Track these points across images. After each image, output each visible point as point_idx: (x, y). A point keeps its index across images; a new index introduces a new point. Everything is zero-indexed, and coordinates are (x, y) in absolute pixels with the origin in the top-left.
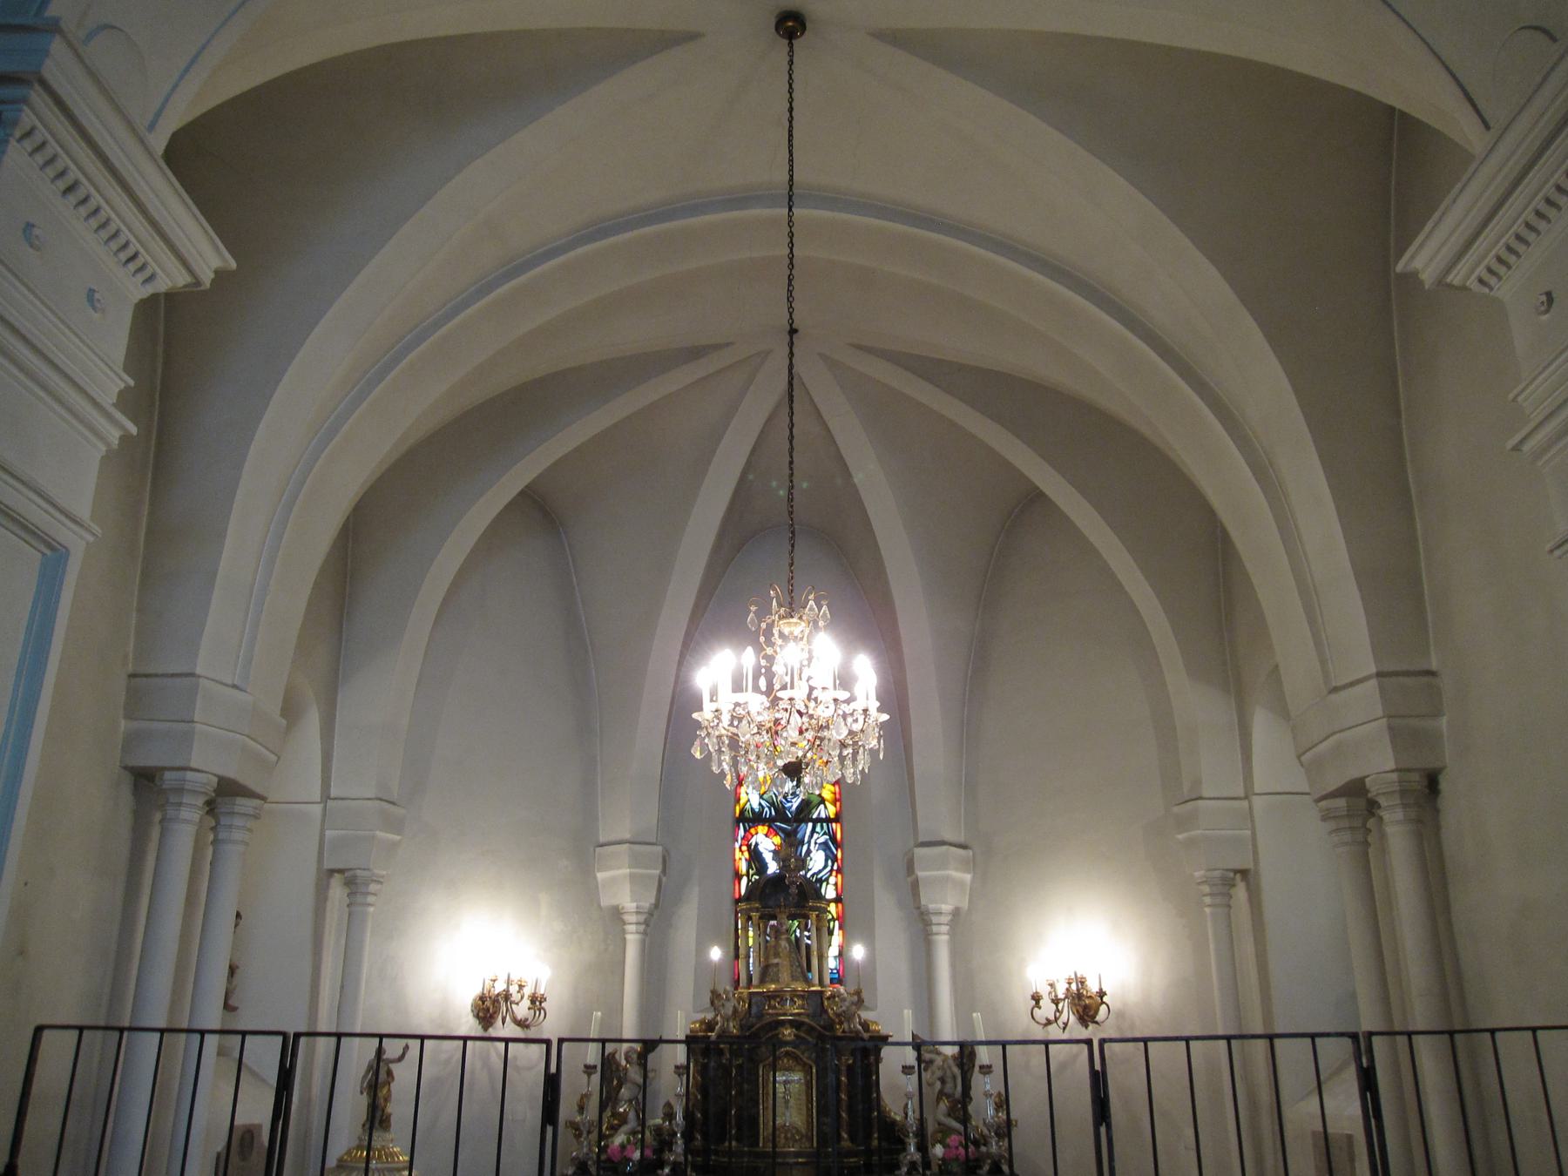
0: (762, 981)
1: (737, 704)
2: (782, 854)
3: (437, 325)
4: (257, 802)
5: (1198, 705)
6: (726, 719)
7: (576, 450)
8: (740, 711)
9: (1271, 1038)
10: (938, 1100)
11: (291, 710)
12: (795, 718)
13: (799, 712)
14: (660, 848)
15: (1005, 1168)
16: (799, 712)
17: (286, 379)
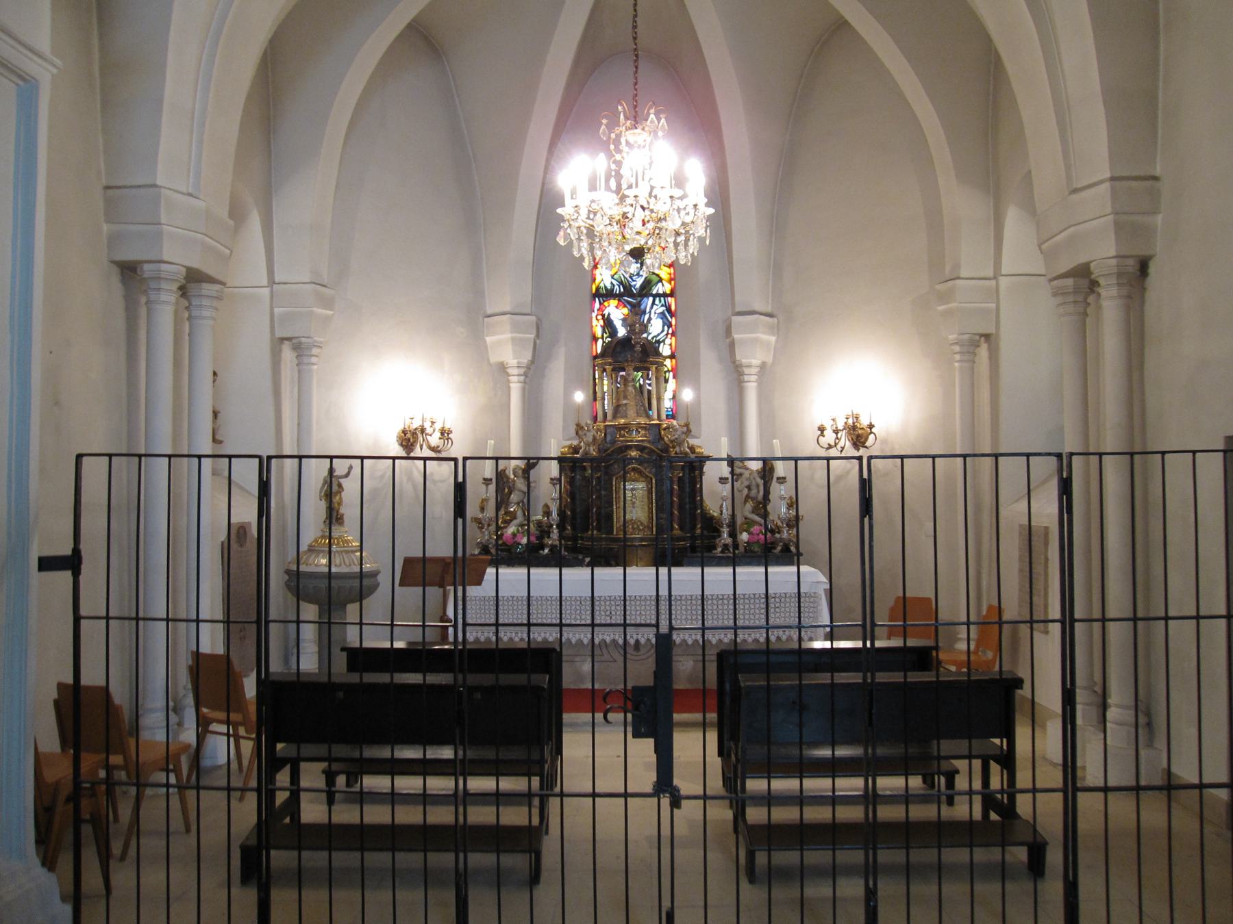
0: (615, 417)
1: (593, 201)
2: (629, 321)
4: (217, 287)
5: (962, 204)
8: (594, 206)
9: (996, 456)
11: (237, 213)
12: (640, 214)
13: (642, 207)
14: (533, 318)
15: (793, 549)
16: (642, 207)
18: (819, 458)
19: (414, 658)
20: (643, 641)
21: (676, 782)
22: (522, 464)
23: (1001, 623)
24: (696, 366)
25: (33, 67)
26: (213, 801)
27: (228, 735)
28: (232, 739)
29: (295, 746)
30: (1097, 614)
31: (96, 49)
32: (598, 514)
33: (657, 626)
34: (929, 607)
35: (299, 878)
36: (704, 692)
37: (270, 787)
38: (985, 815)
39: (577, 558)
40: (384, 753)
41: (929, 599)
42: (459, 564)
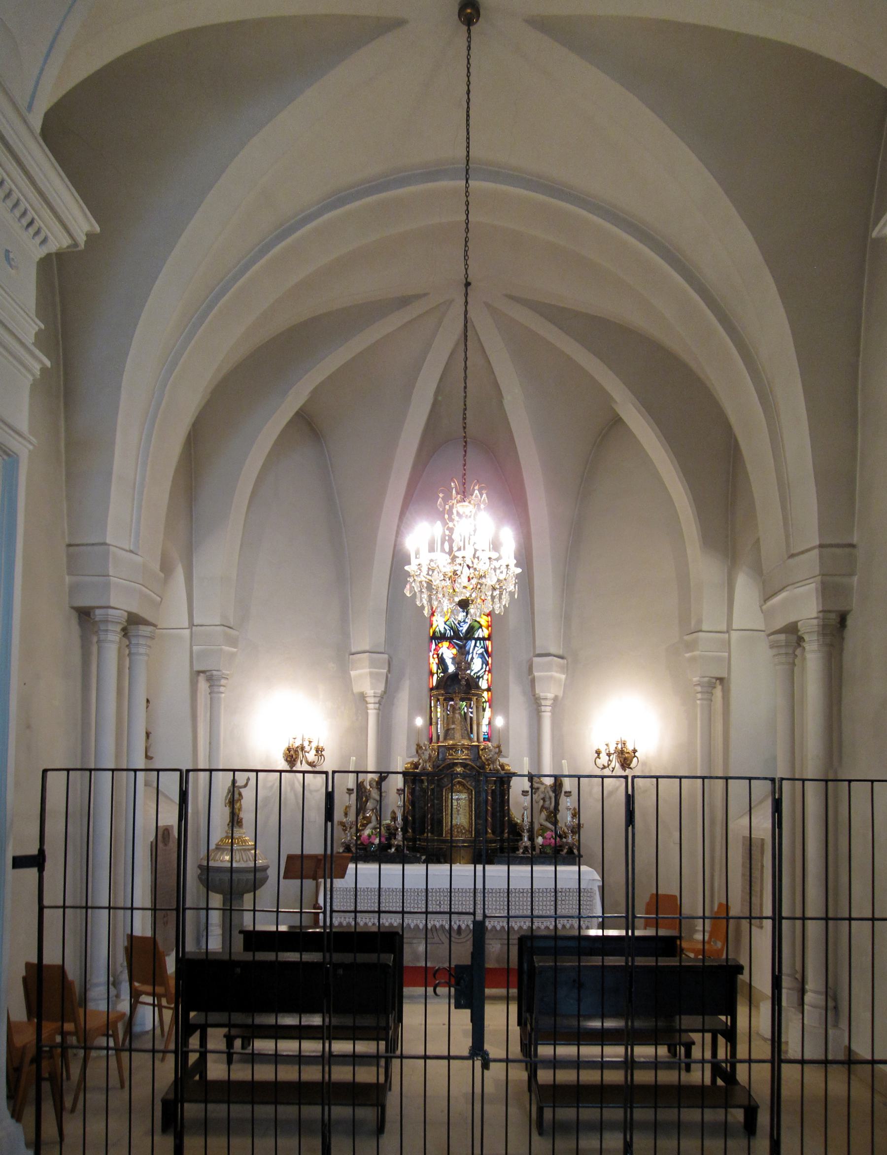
0: (445, 739)
1: (432, 561)
2: (457, 660)
3: (235, 279)
4: (150, 628)
5: (705, 568)
6: (425, 572)
7: (330, 377)
8: (433, 564)
9: (727, 779)
10: (541, 811)
11: (166, 567)
12: (466, 572)
13: (468, 566)
14: (386, 656)
15: (575, 851)
16: (468, 566)
17: (141, 323)
18: (596, 776)
19: (294, 939)
20: (463, 927)
21: (486, 1047)
22: (375, 777)
23: (728, 918)
24: (506, 698)
25: (15, 444)
26: (141, 1060)
27: (154, 1005)
28: (156, 1009)
29: (203, 1014)
30: (799, 914)
31: (63, 430)
32: (432, 819)
33: (474, 914)
34: (675, 903)
35: (205, 1127)
36: (508, 970)
37: (185, 1049)
38: (714, 1081)
39: (415, 856)
40: (269, 1020)
41: (675, 896)
42: (328, 860)
